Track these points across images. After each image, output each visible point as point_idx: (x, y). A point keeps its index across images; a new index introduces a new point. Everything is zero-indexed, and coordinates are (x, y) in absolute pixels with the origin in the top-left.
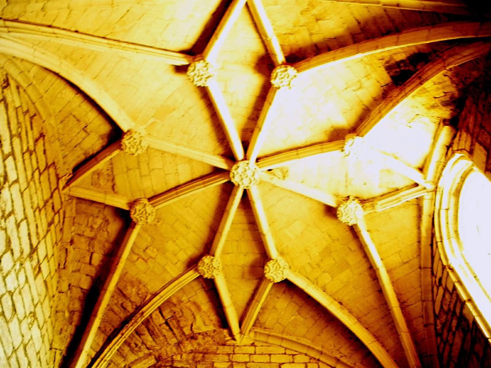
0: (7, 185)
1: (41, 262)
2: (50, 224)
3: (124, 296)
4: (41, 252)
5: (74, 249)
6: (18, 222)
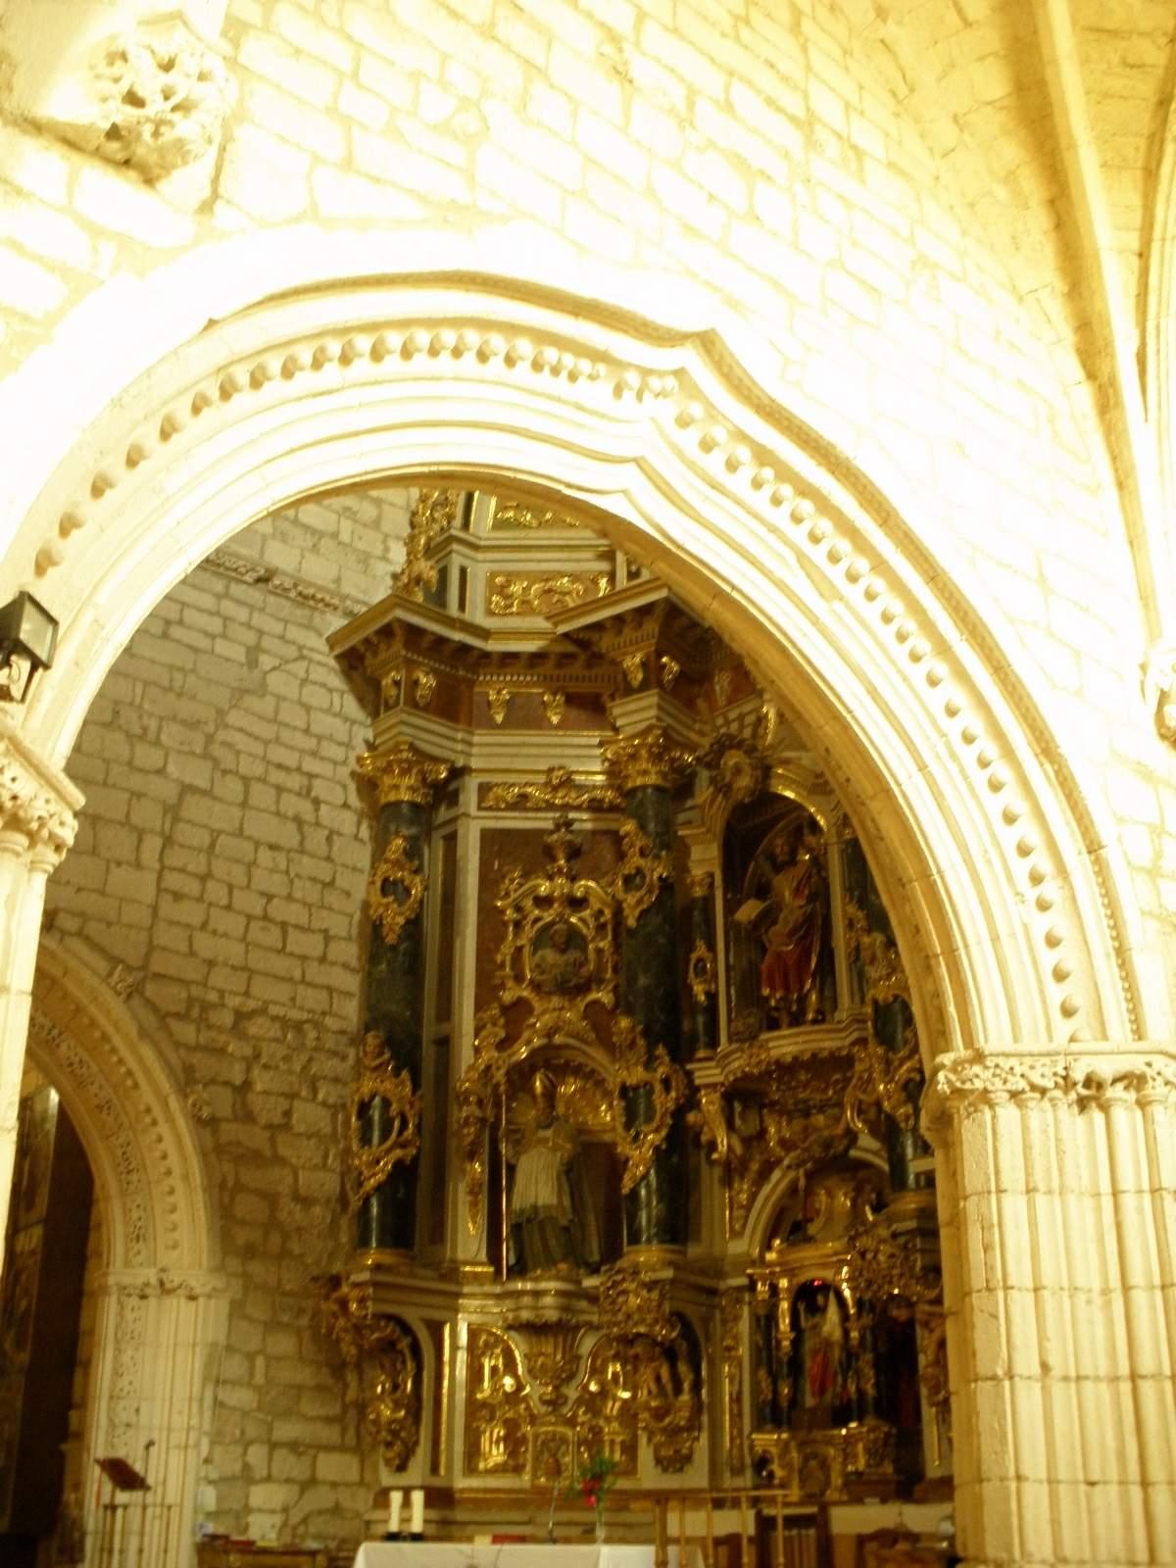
0: (627, 47)
1: (845, 135)
2: (795, 28)
3: (1114, 34)
4: (829, 109)
5: (899, 23)
6: (722, 97)
